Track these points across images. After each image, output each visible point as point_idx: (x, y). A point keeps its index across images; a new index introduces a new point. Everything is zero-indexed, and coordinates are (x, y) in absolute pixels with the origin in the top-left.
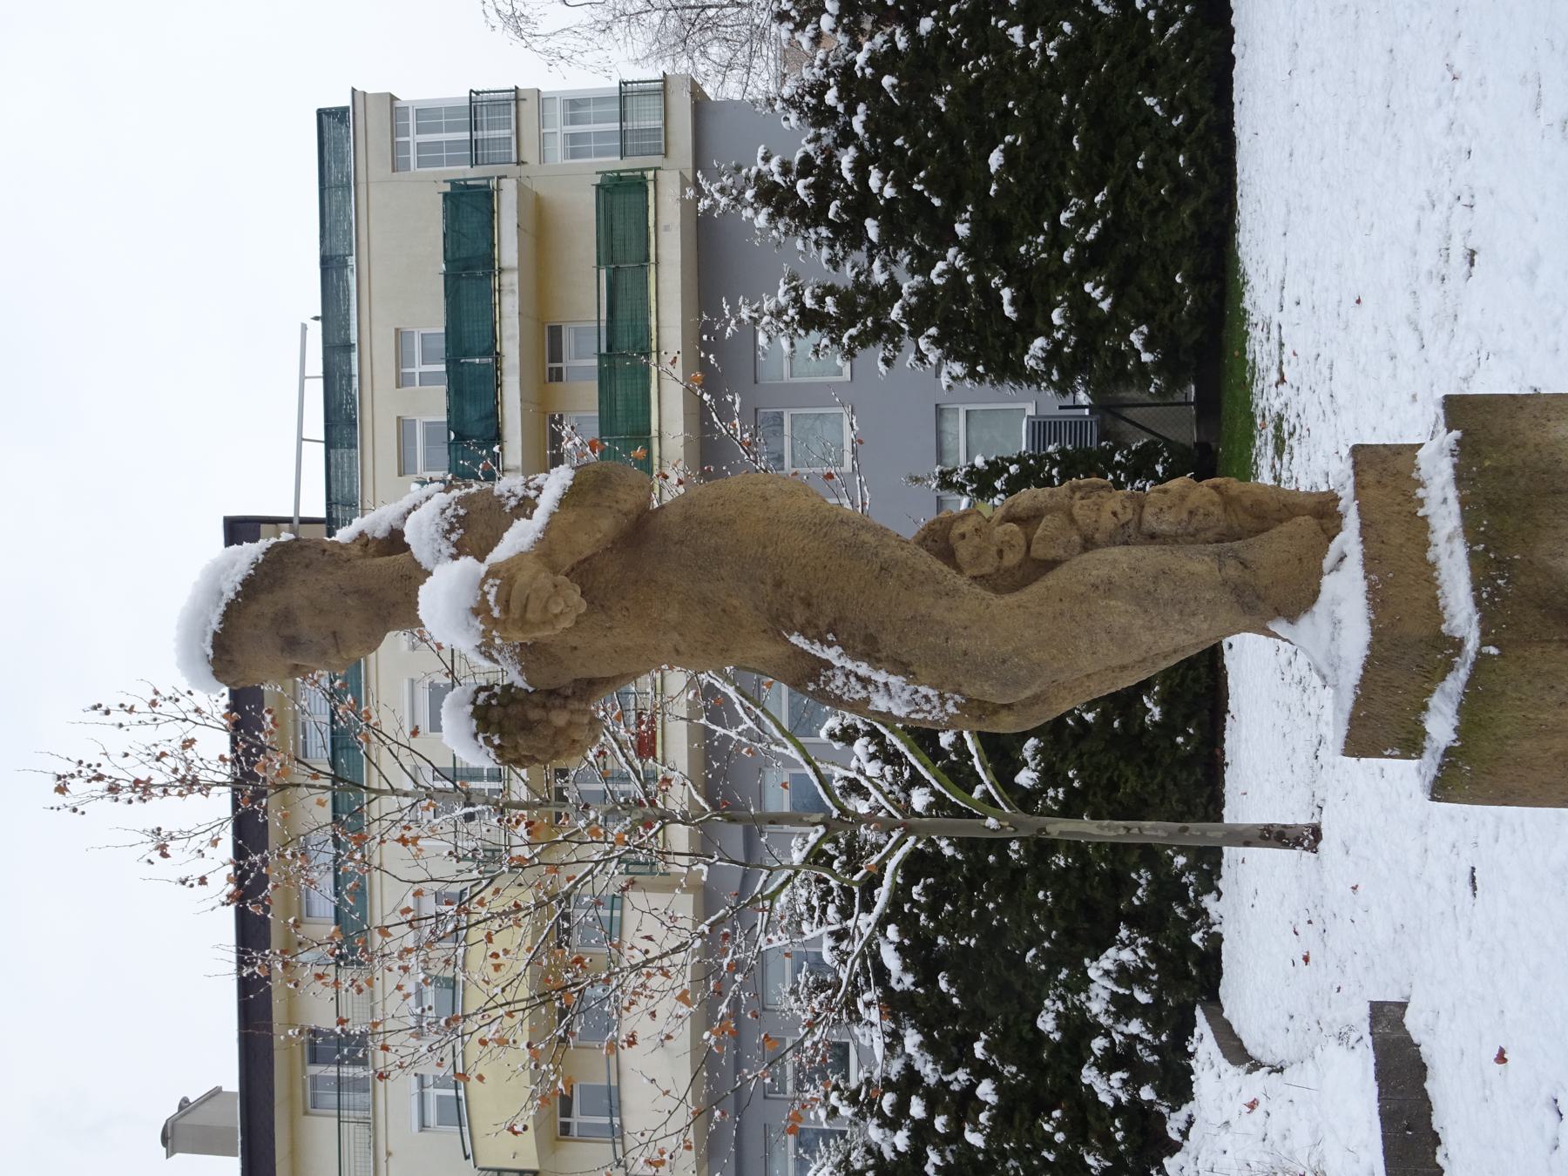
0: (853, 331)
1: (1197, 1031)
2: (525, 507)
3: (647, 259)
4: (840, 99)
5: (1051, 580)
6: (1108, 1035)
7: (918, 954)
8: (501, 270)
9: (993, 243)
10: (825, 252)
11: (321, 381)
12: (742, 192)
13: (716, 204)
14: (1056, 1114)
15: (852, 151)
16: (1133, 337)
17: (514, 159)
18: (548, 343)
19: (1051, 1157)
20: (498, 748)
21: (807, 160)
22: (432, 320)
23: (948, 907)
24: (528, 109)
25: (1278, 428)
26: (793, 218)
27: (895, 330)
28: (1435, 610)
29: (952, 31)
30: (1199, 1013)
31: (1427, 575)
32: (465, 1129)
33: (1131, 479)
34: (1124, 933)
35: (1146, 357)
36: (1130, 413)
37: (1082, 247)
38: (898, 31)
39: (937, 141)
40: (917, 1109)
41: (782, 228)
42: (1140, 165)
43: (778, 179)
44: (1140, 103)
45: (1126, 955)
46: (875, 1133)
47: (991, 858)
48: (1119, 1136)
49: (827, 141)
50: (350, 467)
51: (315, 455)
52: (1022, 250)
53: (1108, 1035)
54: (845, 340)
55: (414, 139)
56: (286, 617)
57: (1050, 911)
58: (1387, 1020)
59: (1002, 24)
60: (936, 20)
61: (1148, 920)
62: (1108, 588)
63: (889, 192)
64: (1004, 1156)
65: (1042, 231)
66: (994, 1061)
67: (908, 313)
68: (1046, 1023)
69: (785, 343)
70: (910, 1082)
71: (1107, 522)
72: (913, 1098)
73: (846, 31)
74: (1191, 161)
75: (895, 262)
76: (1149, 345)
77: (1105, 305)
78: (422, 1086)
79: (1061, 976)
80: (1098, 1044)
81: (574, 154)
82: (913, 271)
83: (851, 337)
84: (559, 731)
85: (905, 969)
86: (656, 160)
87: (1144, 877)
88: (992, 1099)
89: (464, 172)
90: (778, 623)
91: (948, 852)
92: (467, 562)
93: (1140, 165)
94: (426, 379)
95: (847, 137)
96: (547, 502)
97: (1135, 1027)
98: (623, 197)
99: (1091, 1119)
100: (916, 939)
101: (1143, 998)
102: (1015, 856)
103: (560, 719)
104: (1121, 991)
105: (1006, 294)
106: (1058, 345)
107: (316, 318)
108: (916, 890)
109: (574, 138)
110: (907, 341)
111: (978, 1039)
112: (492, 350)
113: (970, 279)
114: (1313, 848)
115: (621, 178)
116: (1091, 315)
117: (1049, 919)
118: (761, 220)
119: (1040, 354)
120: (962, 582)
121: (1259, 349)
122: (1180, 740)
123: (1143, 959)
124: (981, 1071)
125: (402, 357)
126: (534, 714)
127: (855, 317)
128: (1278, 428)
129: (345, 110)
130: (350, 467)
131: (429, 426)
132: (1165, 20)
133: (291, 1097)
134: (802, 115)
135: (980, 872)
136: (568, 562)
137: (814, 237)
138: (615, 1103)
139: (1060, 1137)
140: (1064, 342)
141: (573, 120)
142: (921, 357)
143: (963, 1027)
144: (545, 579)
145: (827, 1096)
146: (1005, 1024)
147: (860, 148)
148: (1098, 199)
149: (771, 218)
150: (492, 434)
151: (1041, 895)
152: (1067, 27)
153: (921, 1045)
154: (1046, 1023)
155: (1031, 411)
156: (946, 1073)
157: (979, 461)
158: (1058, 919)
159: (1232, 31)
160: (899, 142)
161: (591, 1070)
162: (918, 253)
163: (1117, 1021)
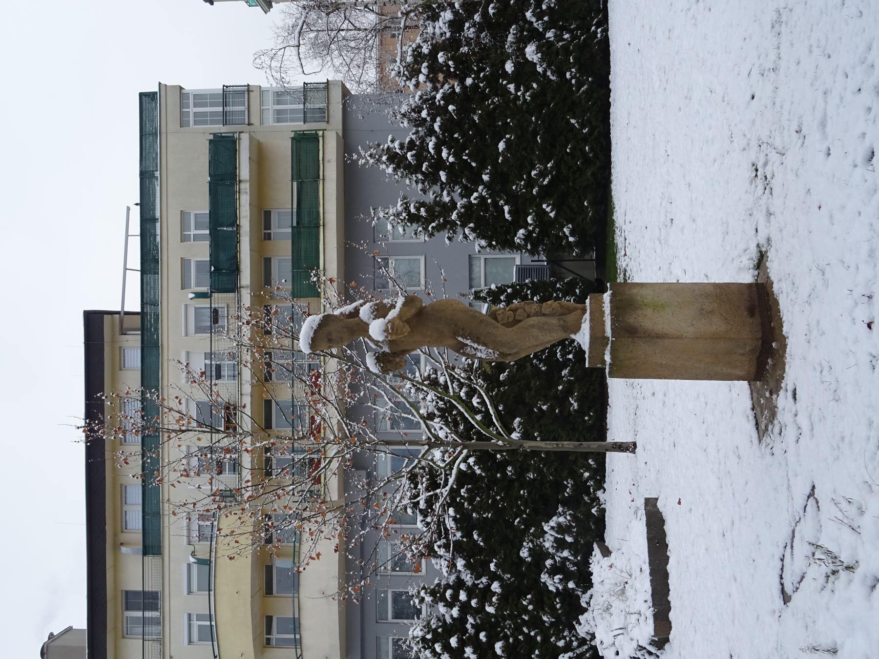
0: (433, 224)
1: (594, 553)
2: (393, 306)
3: (318, 177)
4: (428, 115)
5: (520, 324)
6: (553, 558)
7: (464, 523)
8: (240, 181)
9: (499, 185)
10: (420, 186)
11: (139, 238)
12: (381, 157)
13: (368, 162)
14: (529, 596)
15: (433, 139)
16: (565, 229)
17: (247, 122)
18: (264, 219)
19: (526, 618)
20: (382, 367)
21: (412, 142)
22: (202, 206)
23: (478, 499)
24: (254, 96)
25: (625, 275)
26: (405, 170)
27: (453, 224)
28: (604, 331)
29: (481, 85)
30: (595, 546)
31: (603, 323)
32: (215, 643)
33: (564, 296)
34: (560, 509)
35: (571, 239)
36: (566, 264)
37: (541, 187)
38: (456, 84)
39: (474, 136)
40: (463, 596)
41: (400, 174)
42: (568, 150)
43: (398, 151)
44: (568, 122)
45: (561, 519)
46: (442, 609)
47: (499, 475)
48: (558, 606)
49: (422, 134)
50: (154, 284)
51: (134, 279)
52: (514, 187)
53: (553, 558)
54: (430, 228)
55: (192, 110)
56: (330, 333)
57: (526, 500)
58: (651, 505)
59: (505, 82)
60: (474, 79)
61: (573, 503)
62: (533, 326)
63: (451, 159)
64: (504, 618)
65: (523, 179)
66: (500, 572)
67: (460, 216)
68: (524, 553)
69: (401, 229)
70: (459, 584)
71: (533, 311)
72: (461, 591)
73: (431, 81)
74: (591, 149)
75: (453, 191)
76: (572, 234)
77: (552, 215)
78: (190, 619)
79: (531, 531)
80: (549, 562)
81: (279, 120)
82: (462, 196)
83: (433, 227)
84: (397, 363)
85: (458, 529)
86: (323, 125)
87: (570, 483)
88: (499, 590)
89: (219, 128)
90: (455, 334)
91: (478, 472)
92: (381, 320)
93: (568, 150)
94: (197, 238)
95: (431, 132)
96: (399, 305)
97: (566, 553)
98: (305, 145)
99: (545, 599)
100: (462, 515)
101: (569, 539)
102: (509, 474)
103: (398, 360)
104: (559, 536)
105: (506, 208)
106: (530, 233)
107: (137, 204)
108: (462, 490)
109: (279, 112)
110: (459, 229)
111: (492, 562)
112: (234, 221)
113: (489, 201)
114: (633, 452)
115: (304, 134)
116: (546, 219)
117: (526, 504)
118: (390, 170)
119: (522, 237)
120: (499, 325)
121: (619, 240)
122: (586, 418)
123: (569, 521)
124: (493, 577)
125: (184, 226)
126: (391, 359)
127: (433, 217)
128: (625, 275)
129: (155, 93)
130: (154, 284)
131: (199, 264)
132: (580, 84)
133: (115, 628)
134: (410, 120)
135: (493, 481)
136: (405, 319)
137: (415, 179)
138: (297, 625)
139: (530, 607)
140: (533, 231)
141: (278, 103)
142: (466, 237)
143: (485, 557)
144: (401, 324)
145: (419, 593)
146: (505, 555)
147: (437, 138)
148: (549, 165)
149: (395, 170)
150: (234, 268)
151: (522, 492)
152: (535, 86)
153: (465, 566)
154: (524, 553)
155: (518, 262)
156: (476, 579)
157: (493, 287)
158: (529, 484)
159: (610, 90)
160: (456, 136)
161: (282, 608)
162: (464, 188)
163: (557, 551)
